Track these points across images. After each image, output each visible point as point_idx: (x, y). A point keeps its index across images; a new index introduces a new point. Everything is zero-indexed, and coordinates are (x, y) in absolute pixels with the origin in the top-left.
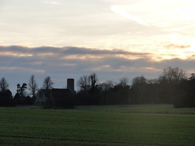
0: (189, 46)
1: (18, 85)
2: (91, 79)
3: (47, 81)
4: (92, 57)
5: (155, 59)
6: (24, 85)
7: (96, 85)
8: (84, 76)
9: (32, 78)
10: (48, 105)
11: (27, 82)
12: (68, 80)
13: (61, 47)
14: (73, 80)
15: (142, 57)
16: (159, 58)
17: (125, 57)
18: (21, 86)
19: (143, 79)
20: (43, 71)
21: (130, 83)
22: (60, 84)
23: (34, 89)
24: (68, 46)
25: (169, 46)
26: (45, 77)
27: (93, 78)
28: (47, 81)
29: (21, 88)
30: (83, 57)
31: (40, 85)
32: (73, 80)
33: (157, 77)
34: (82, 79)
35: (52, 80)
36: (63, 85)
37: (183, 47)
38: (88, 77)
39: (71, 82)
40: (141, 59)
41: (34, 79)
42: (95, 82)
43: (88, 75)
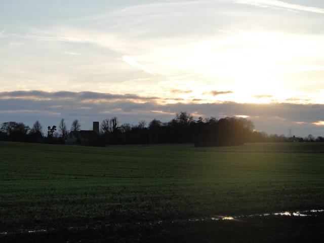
0: (191, 91)
1: (49, 127)
2: (112, 122)
3: (75, 123)
4: (103, 100)
5: (159, 102)
6: (54, 127)
7: (117, 128)
8: (106, 120)
9: (63, 121)
10: (78, 142)
11: (58, 124)
12: (94, 123)
13: (78, 92)
14: (98, 123)
15: (149, 102)
16: (164, 102)
17: (135, 101)
18: (51, 128)
19: (321, 137)
20: (59, 114)
21: (147, 126)
22: (87, 126)
23: (64, 130)
24: (84, 90)
25: (215, 93)
26: (74, 120)
27: (114, 120)
28: (75, 123)
29: (52, 130)
30: (97, 101)
31: (69, 128)
32: (98, 123)
33: (169, 120)
34: (104, 122)
35: (80, 123)
36: (90, 127)
37: (186, 92)
38: (109, 121)
39: (96, 124)
40: (147, 103)
41: (64, 122)
42: (116, 124)
43: (110, 118)
